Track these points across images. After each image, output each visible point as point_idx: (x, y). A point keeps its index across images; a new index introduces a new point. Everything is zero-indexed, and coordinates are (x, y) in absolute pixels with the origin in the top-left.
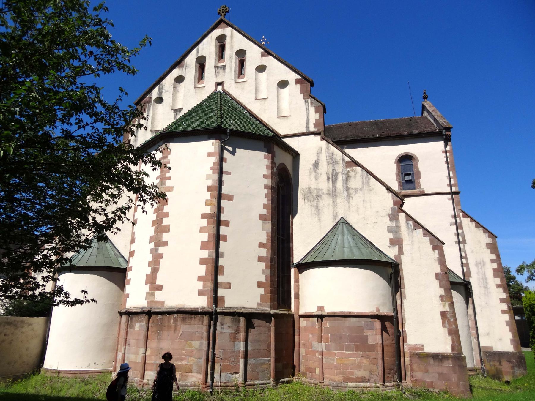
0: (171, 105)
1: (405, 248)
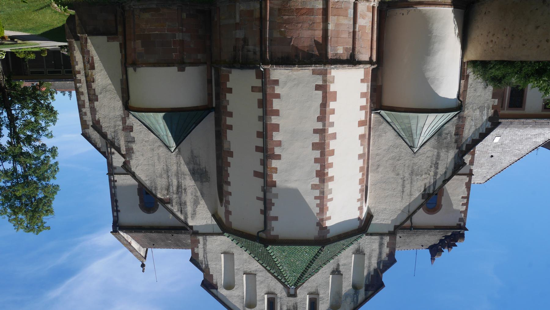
0: (343, 280)
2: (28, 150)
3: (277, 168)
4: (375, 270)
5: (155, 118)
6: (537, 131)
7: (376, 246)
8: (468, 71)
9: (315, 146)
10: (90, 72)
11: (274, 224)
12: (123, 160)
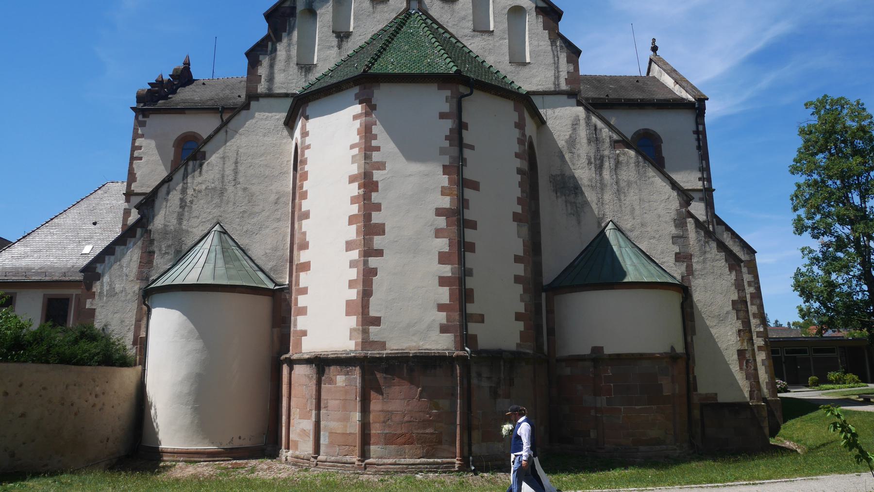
0: (331, 23)
2: (841, 228)
3: (442, 195)
4: (279, 39)
5: (640, 273)
6: (23, 263)
7: (279, 77)
8: (134, 351)
9: (380, 230)
10: (745, 346)
11: (446, 108)
12: (689, 208)
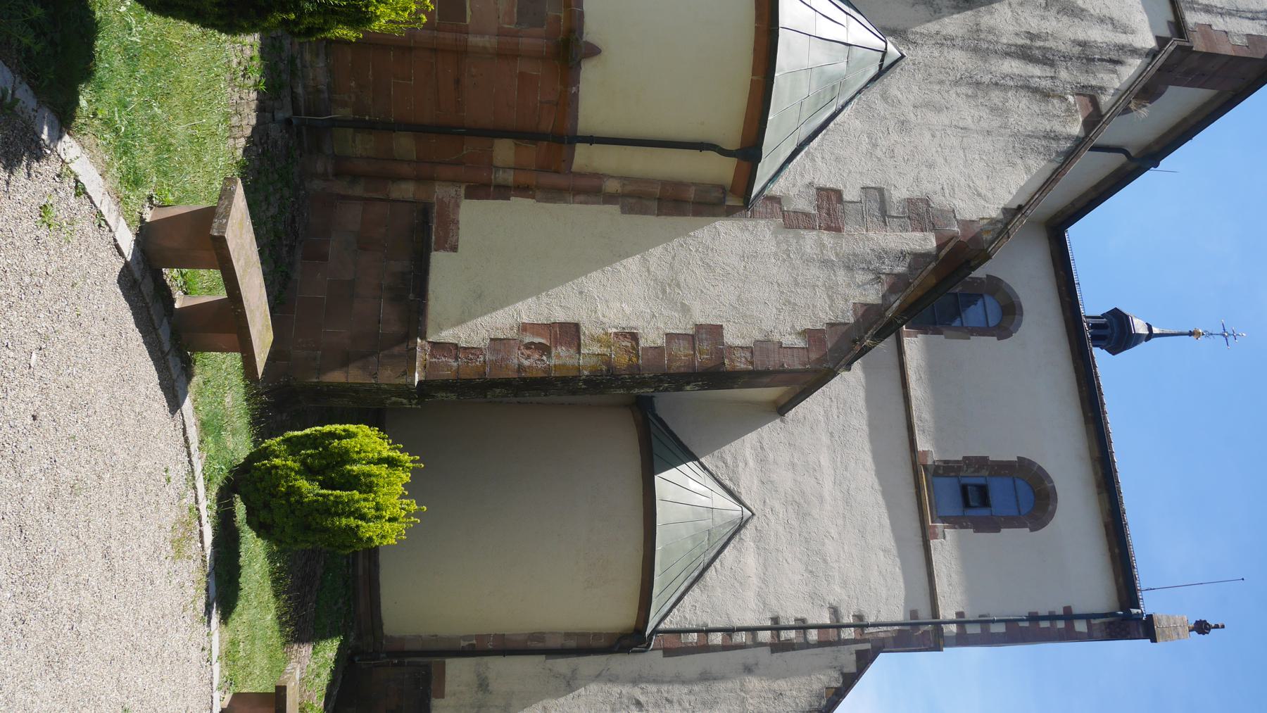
1: (810, 240)
